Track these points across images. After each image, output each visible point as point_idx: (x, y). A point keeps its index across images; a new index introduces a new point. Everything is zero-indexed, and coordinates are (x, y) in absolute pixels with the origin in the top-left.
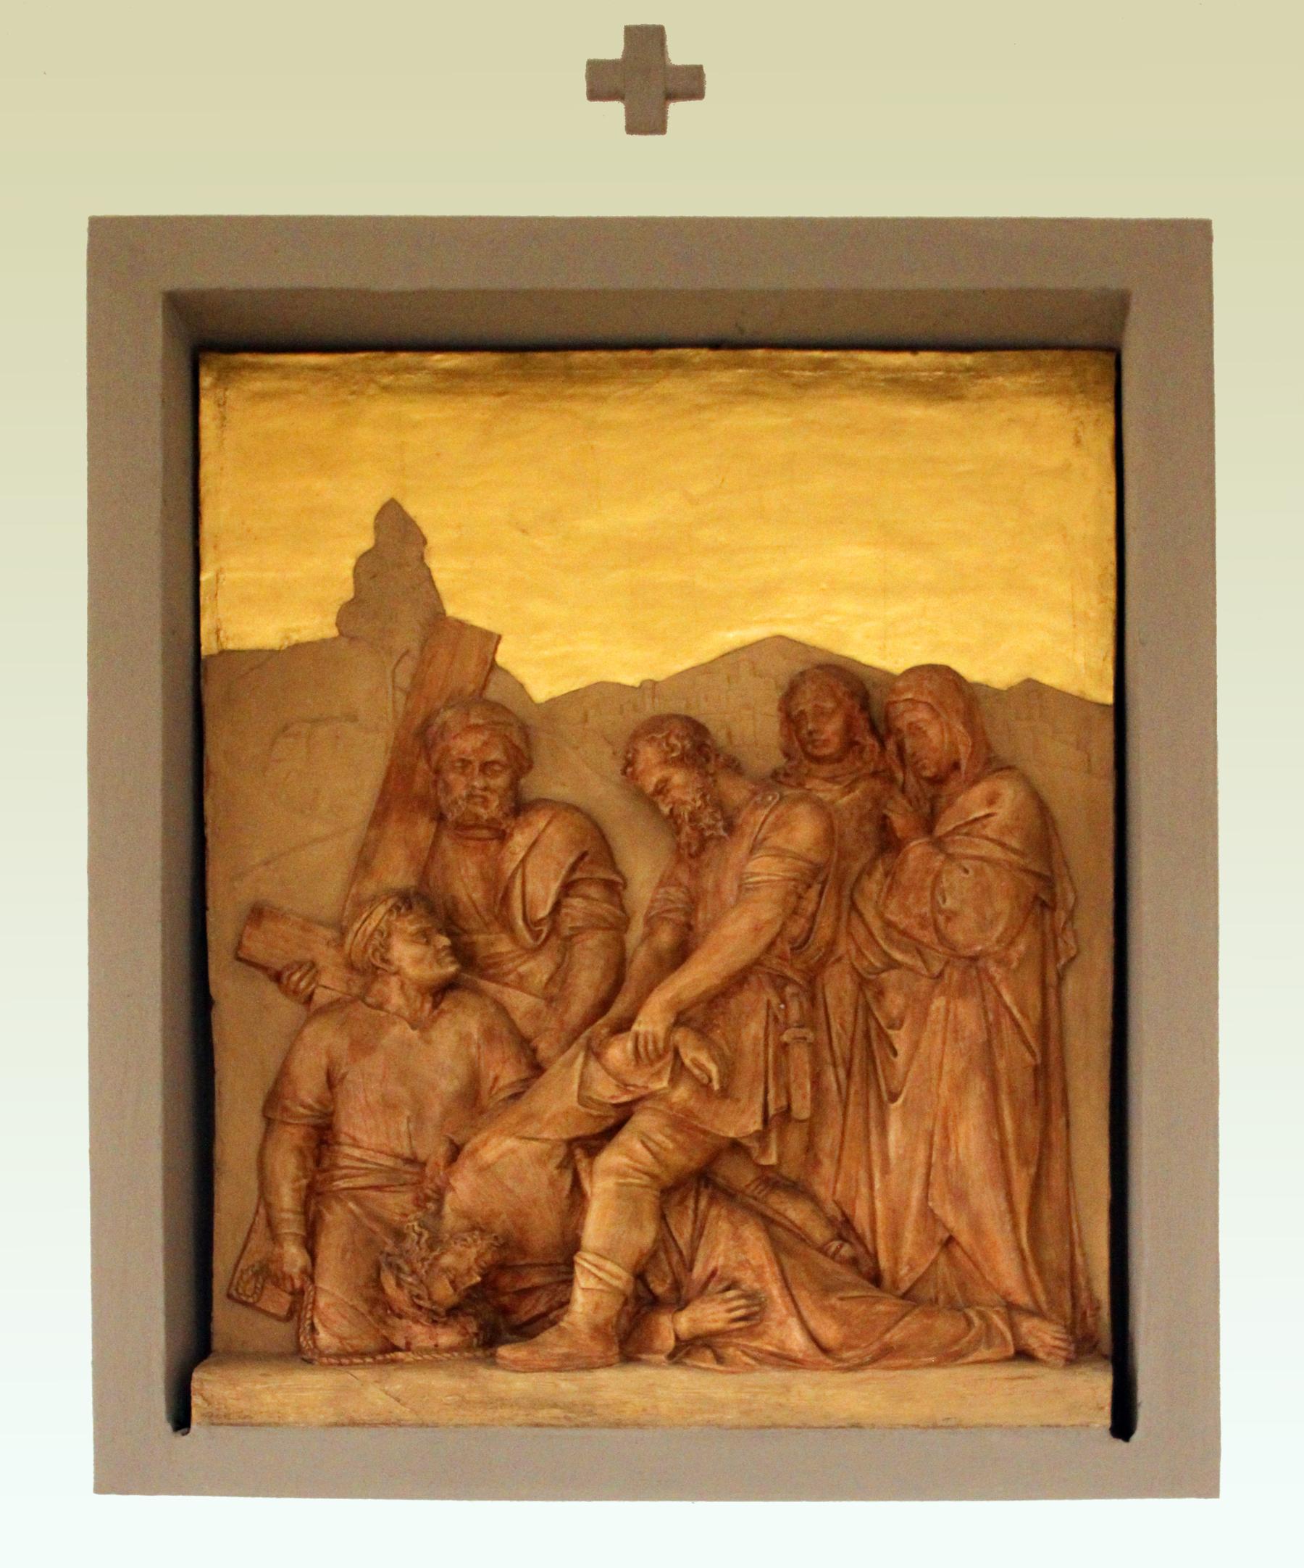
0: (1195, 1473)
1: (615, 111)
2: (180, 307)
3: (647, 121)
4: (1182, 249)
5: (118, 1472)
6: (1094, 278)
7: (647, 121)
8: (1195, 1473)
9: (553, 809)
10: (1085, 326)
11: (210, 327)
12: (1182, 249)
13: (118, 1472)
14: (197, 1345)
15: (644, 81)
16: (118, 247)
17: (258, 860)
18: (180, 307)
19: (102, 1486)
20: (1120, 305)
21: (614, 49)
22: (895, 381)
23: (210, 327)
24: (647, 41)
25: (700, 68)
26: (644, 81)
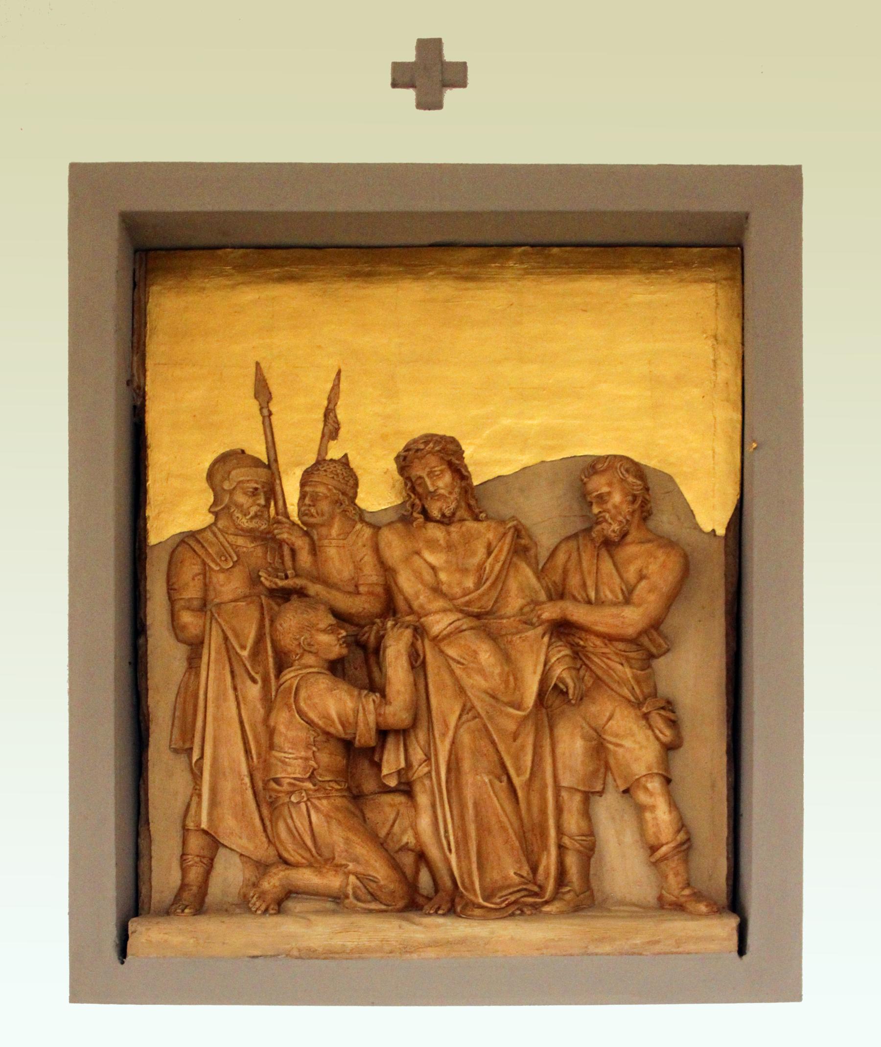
0: (785, 985)
1: (410, 95)
2: (131, 224)
3: (430, 102)
4: (782, 186)
5: (83, 989)
6: (726, 203)
7: (430, 102)
8: (785, 985)
9: (638, 787)
10: (716, 238)
11: (156, 246)
12: (782, 186)
13: (83, 989)
14: (135, 904)
15: (430, 75)
16: (87, 181)
17: (363, 598)
18: (131, 224)
19: (73, 166)
20: (742, 221)
21: (409, 56)
22: (500, 462)
23: (156, 246)
24: (430, 48)
25: (465, 64)
26: (430, 75)
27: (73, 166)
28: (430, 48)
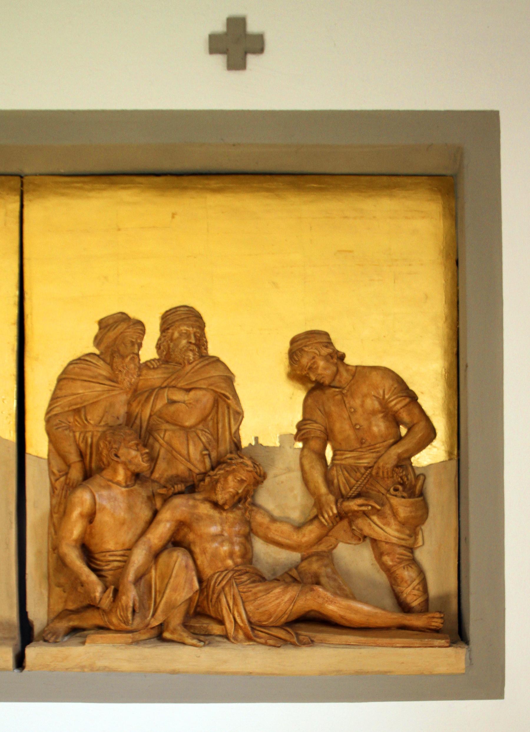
3: (237, 64)
7: (237, 64)
15: (236, 44)
19: (500, 695)
24: (237, 24)
27: (500, 695)
28: (237, 24)
